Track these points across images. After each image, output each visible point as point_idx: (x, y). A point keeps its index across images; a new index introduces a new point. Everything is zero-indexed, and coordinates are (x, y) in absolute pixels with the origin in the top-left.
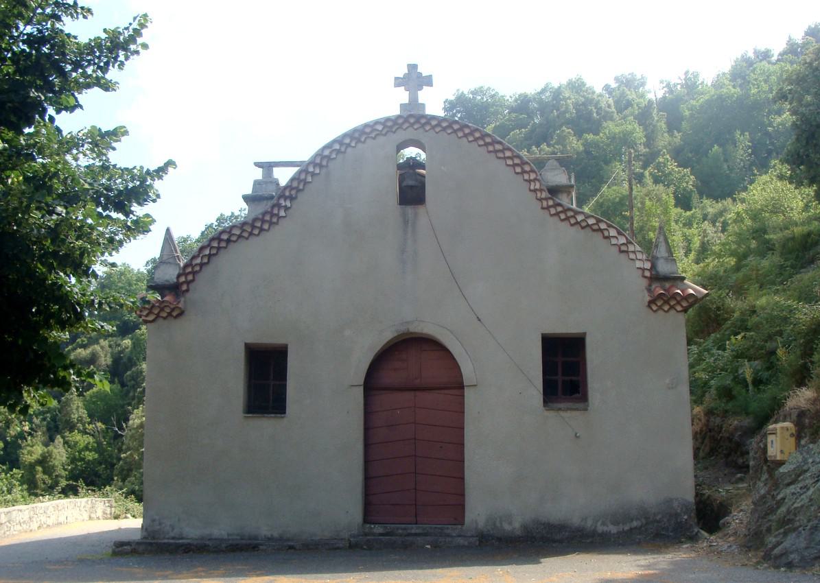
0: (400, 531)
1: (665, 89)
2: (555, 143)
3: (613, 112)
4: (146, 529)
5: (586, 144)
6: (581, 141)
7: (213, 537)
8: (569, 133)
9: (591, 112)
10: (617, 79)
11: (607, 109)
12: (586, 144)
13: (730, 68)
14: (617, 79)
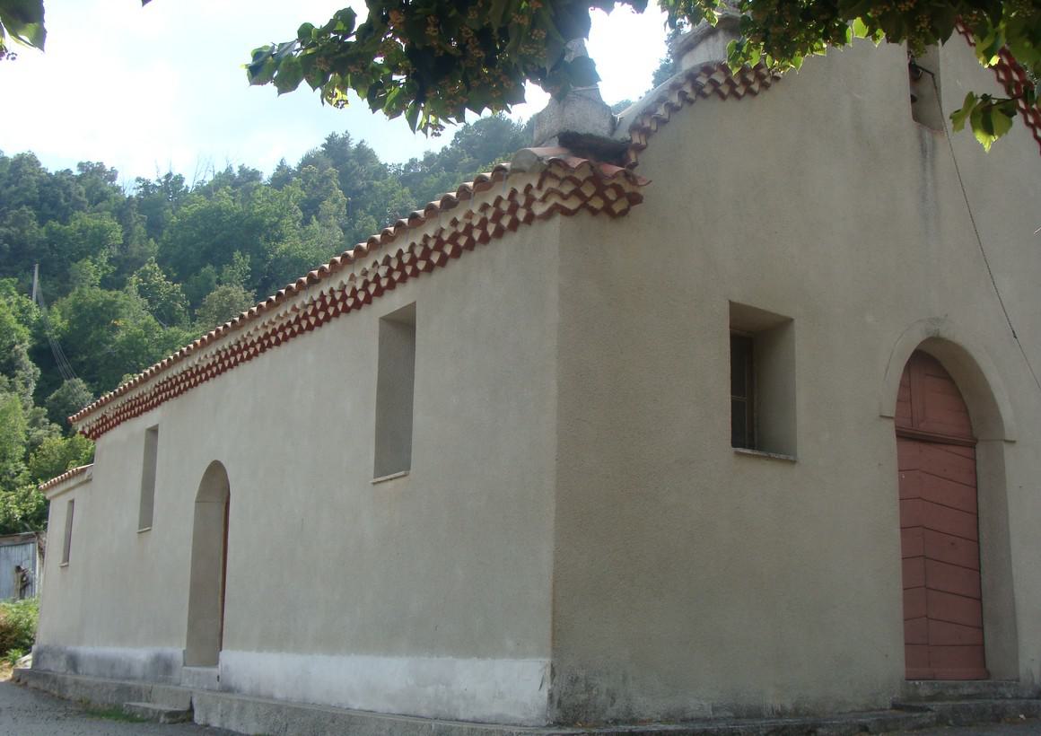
0: (951, 692)
1: (141, 190)
2: (11, 225)
3: (84, 202)
4: (560, 702)
5: (50, 232)
6: (44, 229)
7: (689, 715)
8: (30, 215)
9: (57, 197)
10: (81, 166)
11: (78, 197)
12: (50, 232)
13: (405, 161)
14: (81, 166)
